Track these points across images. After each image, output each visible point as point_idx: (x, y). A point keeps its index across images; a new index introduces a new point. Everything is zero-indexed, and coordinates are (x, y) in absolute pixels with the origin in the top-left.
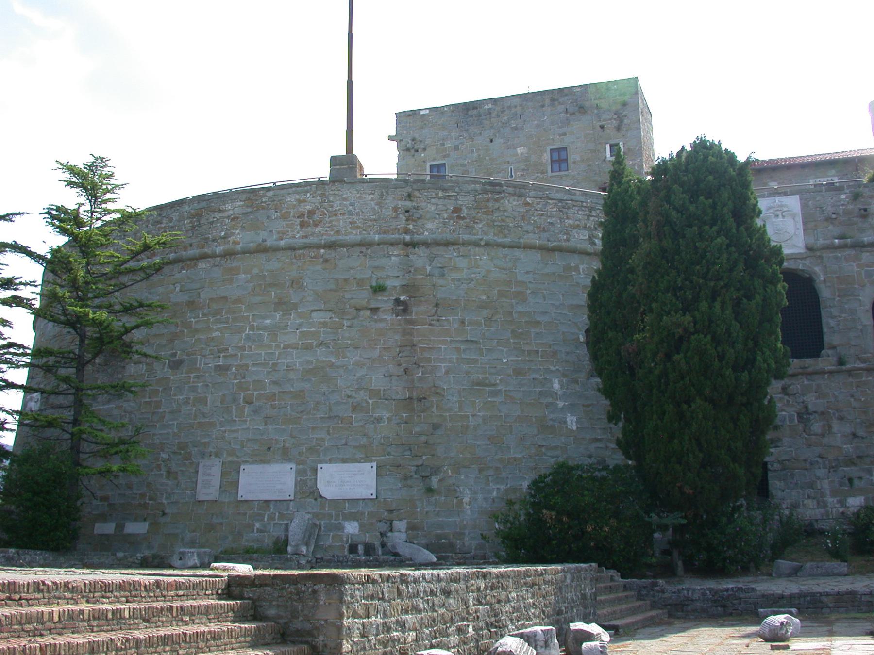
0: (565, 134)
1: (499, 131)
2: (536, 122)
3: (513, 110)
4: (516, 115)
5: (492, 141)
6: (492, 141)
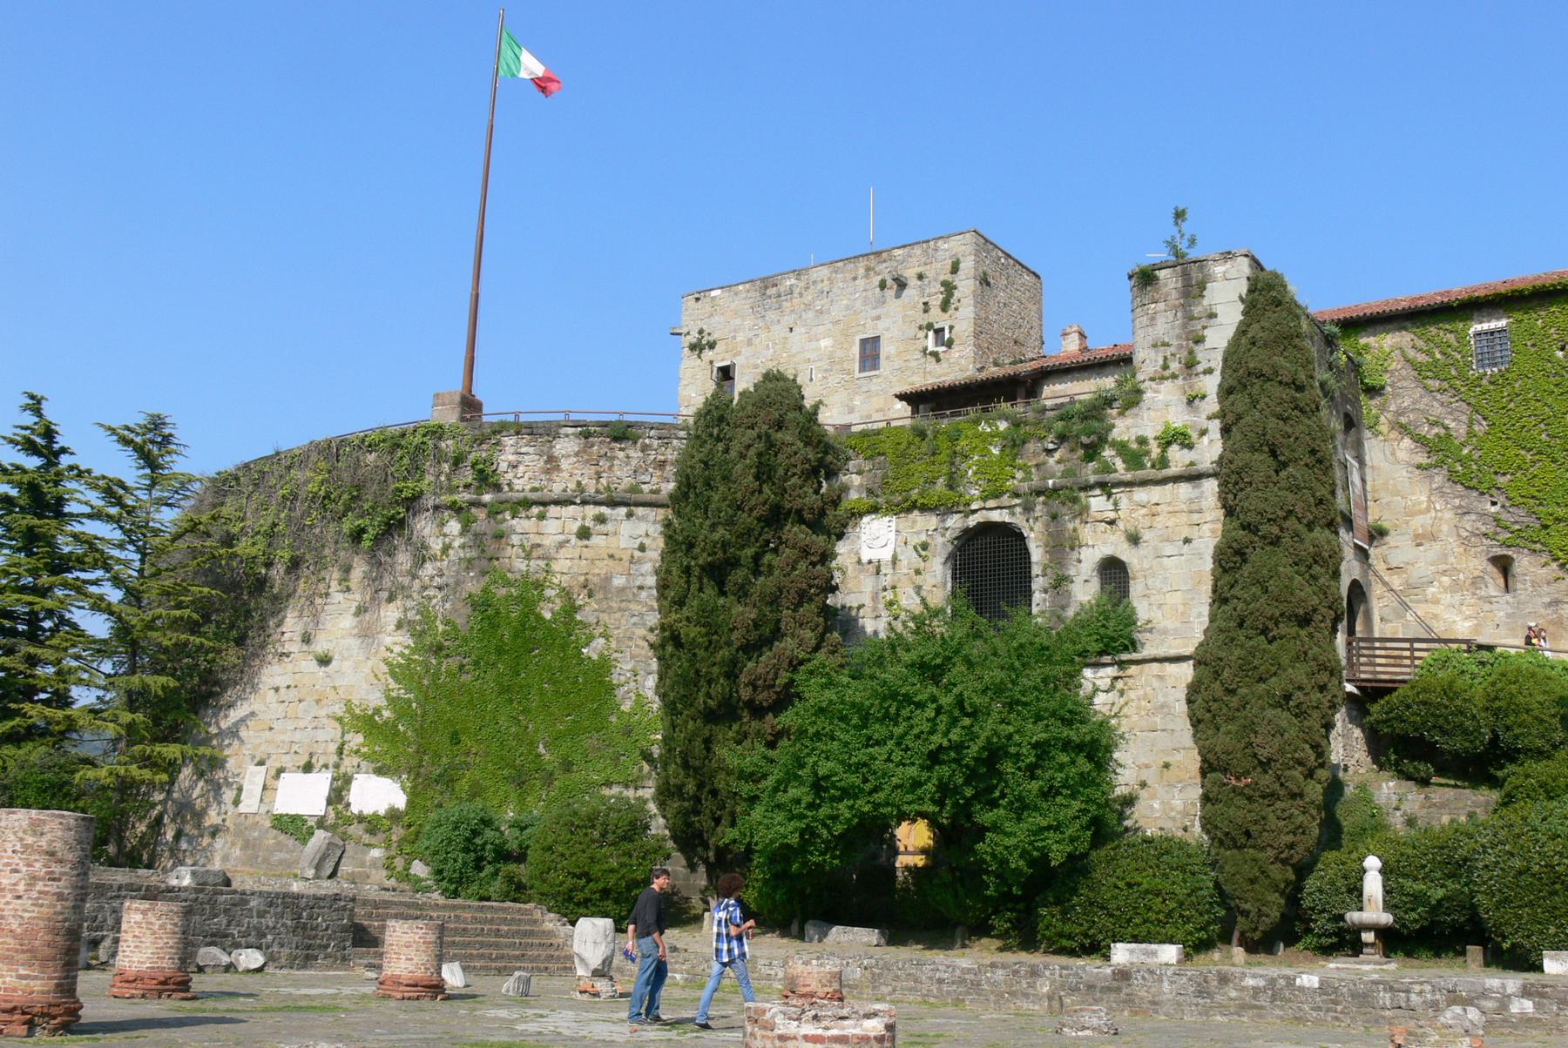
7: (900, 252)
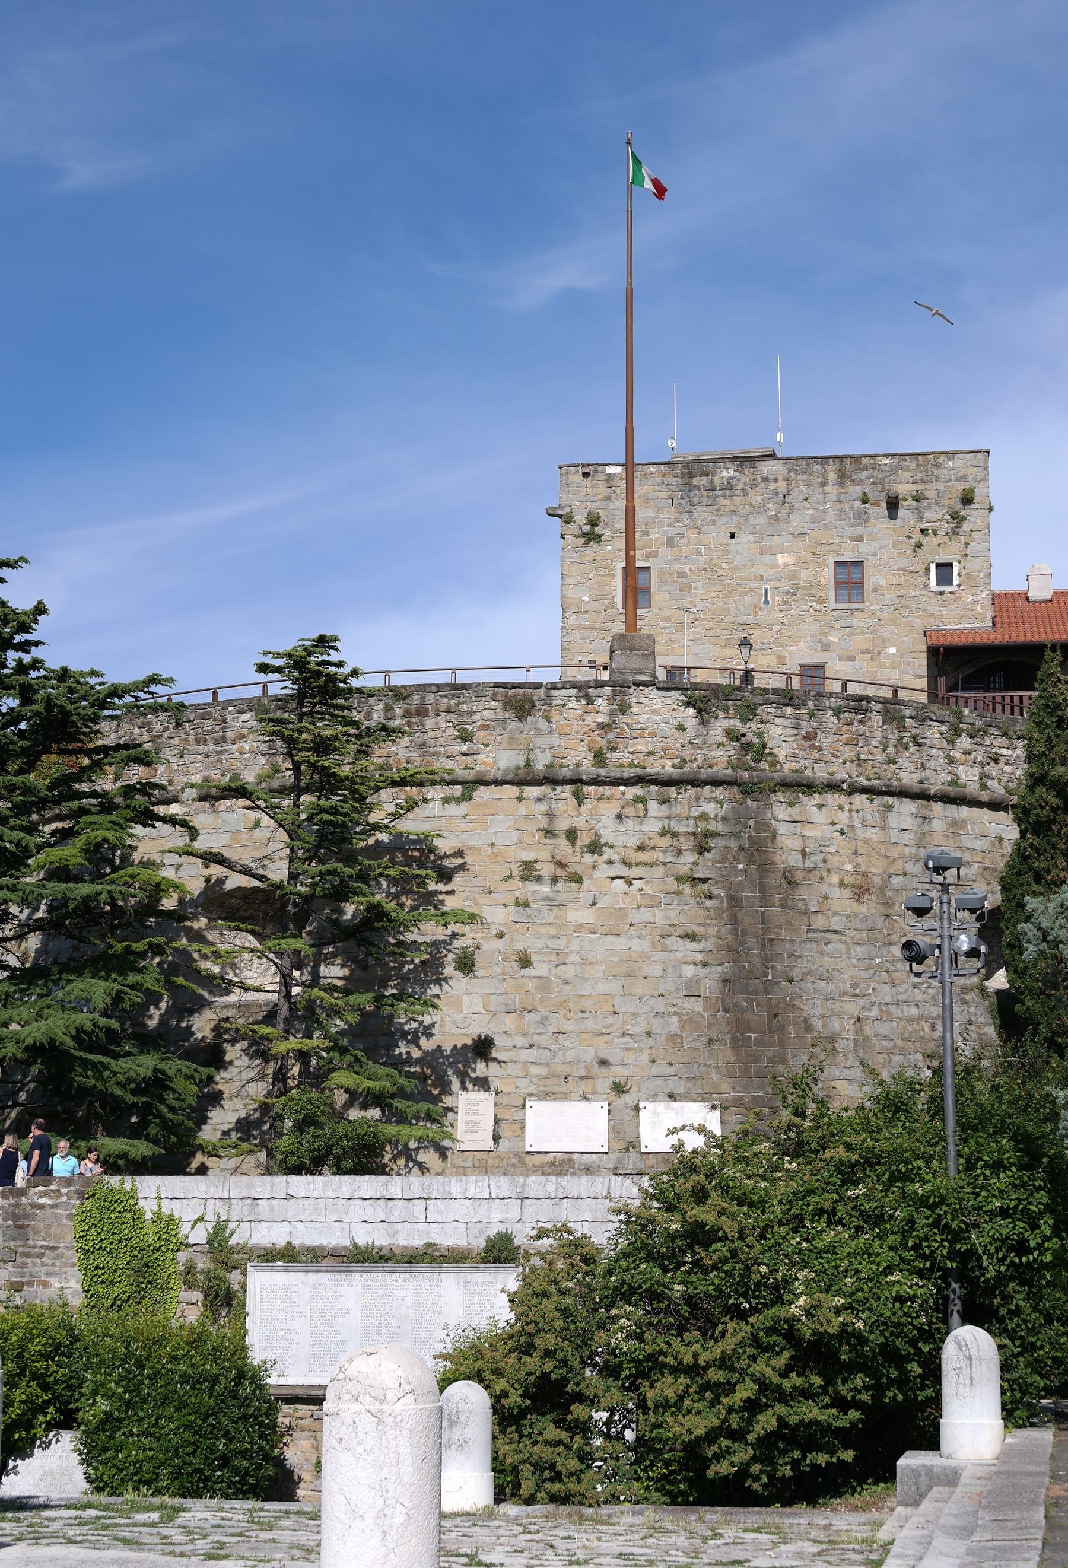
0: (860, 538)
1: (746, 521)
2: (811, 511)
3: (772, 486)
4: (777, 494)
5: (733, 536)
6: (733, 536)
7: (887, 461)
